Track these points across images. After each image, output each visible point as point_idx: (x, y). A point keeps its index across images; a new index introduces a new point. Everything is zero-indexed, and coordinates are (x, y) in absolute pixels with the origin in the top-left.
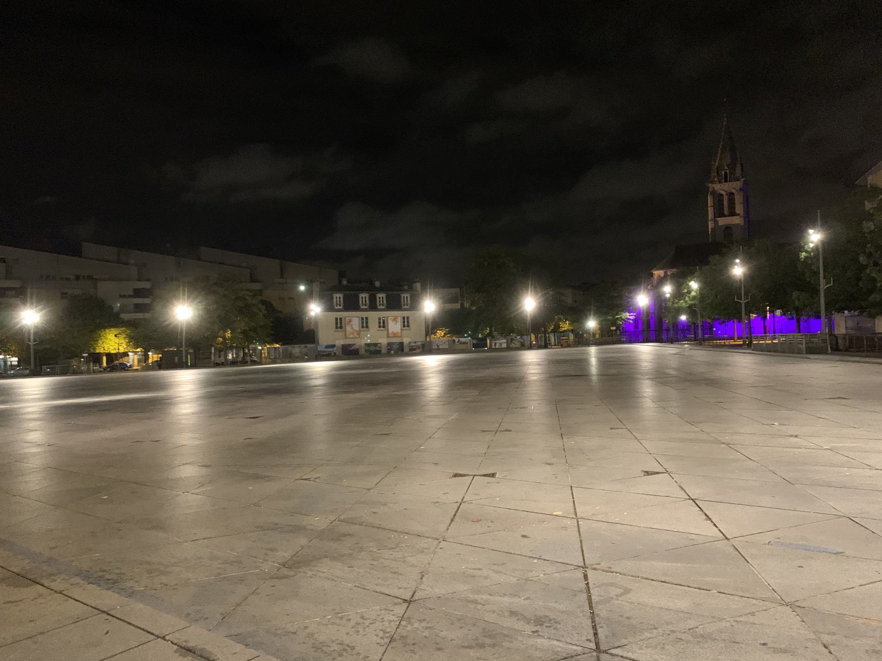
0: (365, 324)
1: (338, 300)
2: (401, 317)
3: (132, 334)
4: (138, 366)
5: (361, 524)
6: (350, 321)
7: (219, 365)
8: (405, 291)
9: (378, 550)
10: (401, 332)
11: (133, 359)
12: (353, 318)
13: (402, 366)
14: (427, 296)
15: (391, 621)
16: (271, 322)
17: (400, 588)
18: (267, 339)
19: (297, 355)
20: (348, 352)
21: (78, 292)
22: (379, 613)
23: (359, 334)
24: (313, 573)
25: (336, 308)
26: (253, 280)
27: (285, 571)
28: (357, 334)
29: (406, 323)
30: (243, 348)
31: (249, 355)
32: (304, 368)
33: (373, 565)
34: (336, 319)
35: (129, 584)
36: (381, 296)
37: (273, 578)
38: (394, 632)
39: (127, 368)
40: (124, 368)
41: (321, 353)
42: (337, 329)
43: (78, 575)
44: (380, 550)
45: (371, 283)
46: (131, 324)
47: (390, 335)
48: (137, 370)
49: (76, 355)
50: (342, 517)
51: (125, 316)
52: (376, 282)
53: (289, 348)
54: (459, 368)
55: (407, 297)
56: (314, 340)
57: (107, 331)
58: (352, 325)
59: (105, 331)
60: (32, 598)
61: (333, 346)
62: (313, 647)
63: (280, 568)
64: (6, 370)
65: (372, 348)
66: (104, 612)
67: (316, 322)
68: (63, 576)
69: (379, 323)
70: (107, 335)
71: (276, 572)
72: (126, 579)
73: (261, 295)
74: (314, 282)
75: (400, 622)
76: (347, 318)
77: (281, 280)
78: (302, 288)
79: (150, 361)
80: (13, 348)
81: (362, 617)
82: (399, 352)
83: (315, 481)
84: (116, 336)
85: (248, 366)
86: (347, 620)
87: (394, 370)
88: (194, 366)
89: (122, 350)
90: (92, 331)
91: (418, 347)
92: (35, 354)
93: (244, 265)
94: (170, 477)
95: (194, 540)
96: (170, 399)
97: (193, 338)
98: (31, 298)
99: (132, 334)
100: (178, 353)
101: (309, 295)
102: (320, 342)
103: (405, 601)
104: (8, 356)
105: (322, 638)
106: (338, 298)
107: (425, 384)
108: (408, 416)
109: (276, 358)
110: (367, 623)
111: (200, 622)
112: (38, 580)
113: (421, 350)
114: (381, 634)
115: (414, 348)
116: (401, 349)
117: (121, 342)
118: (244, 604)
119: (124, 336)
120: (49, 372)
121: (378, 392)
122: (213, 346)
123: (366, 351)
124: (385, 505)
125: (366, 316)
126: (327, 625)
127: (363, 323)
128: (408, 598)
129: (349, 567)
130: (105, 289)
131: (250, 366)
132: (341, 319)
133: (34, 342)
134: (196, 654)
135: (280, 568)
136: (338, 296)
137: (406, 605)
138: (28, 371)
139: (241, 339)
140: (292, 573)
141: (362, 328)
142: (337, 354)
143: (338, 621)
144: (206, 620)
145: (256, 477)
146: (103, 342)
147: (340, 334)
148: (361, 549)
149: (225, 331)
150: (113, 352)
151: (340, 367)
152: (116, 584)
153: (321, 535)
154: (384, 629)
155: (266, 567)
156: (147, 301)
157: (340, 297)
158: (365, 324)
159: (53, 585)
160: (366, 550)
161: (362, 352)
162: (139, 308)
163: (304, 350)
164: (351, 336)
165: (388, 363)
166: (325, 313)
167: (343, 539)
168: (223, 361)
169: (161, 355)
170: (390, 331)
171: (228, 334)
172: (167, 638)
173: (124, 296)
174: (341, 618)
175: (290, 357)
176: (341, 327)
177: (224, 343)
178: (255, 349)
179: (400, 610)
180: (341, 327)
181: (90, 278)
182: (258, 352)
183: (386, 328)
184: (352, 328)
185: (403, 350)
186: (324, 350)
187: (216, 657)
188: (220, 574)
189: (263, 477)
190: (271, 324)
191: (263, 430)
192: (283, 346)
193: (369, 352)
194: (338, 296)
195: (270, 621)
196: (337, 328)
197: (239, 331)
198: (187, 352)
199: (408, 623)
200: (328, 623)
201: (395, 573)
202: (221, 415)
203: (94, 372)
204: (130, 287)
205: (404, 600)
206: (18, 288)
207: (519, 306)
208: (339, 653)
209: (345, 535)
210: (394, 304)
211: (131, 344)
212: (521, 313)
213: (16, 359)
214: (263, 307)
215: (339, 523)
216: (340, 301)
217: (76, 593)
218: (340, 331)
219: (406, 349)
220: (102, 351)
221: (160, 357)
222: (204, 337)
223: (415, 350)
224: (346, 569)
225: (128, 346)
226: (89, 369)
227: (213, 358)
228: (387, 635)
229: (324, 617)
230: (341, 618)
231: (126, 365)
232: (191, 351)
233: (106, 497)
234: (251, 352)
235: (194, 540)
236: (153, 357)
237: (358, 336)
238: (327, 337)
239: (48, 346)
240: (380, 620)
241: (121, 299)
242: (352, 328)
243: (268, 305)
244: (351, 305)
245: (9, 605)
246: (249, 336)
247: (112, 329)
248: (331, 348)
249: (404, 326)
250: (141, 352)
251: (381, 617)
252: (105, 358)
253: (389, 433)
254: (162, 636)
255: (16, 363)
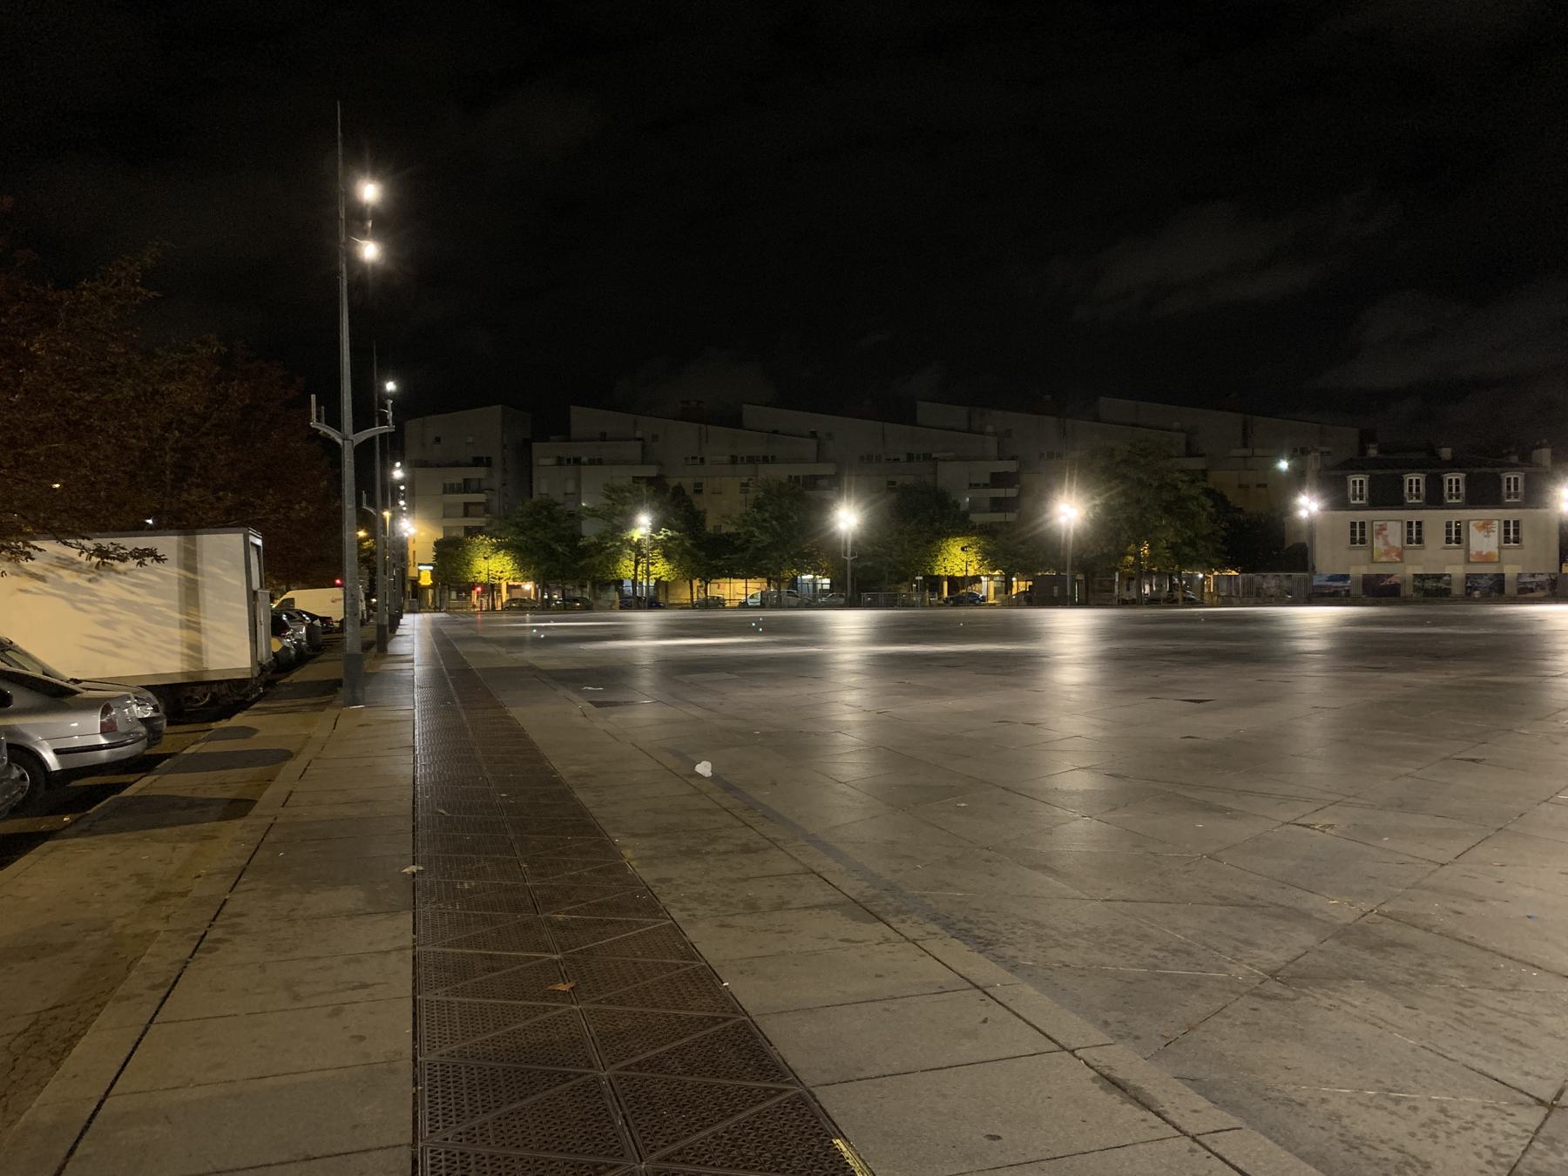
0: (1415, 535)
1: (1358, 487)
2: (1499, 520)
3: (987, 547)
4: (995, 598)
5: (1427, 929)
6: (1383, 528)
7: (1127, 604)
8: (1512, 466)
9: (1470, 987)
10: (1500, 552)
11: (987, 587)
12: (1389, 524)
13: (1504, 624)
14: (1062, 493)
15: (1510, 1134)
16: (1224, 529)
17: (1527, 1074)
18: (1215, 561)
19: (1272, 591)
20: (1376, 590)
21: (909, 480)
22: (1480, 1111)
23: (1400, 555)
24: (1331, 1002)
25: (1352, 502)
26: (1189, 453)
27: (1274, 988)
28: (1396, 556)
29: (1511, 534)
30: (1171, 576)
31: (1180, 589)
32: (1288, 617)
33: (1461, 1014)
34: (1353, 524)
35: (1010, 951)
36: (1456, 479)
37: (1254, 995)
38: (1518, 1157)
39: (977, 602)
40: (975, 601)
41: (1319, 591)
42: (1411, 543)
43: (935, 920)
44: (1474, 987)
45: (1432, 452)
46: (987, 532)
47: (1471, 560)
48: (994, 604)
49: (905, 578)
50: (1386, 909)
51: (977, 518)
52: (1444, 450)
53: (1256, 577)
54: (907, 629)
55: (1516, 479)
56: (1306, 565)
57: (951, 541)
58: (1387, 536)
59: (947, 541)
60: (876, 942)
61: (1345, 577)
62: (1343, 1142)
63: (1266, 980)
64: (815, 597)
65: (1429, 584)
66: (978, 987)
67: (1311, 526)
68: (915, 918)
69: (1449, 532)
70: (950, 547)
71: (1258, 985)
72: (1004, 942)
73: (1205, 481)
74: (1309, 452)
75: (1531, 1142)
76: (1375, 523)
77: (1243, 452)
78: (1284, 465)
79: (1014, 592)
80: (825, 565)
81: (1443, 1111)
82: (1493, 594)
83: (1323, 832)
84: (963, 549)
85: (1178, 607)
86: (1409, 1108)
87: (1482, 631)
88: (1084, 603)
89: (971, 573)
90: (929, 542)
91: (1540, 586)
92: (852, 574)
93: (1176, 425)
94: (1059, 787)
95: (1107, 900)
96: (188, 655)
97: (1084, 556)
98: (850, 484)
99: (987, 547)
100: (1059, 580)
101: (1297, 480)
102: (1318, 569)
103: (1541, 1102)
104: (818, 577)
105: (1360, 1129)
106: (1358, 482)
107: (1560, 664)
108: (1522, 727)
109: (1230, 596)
110: (1454, 1124)
111: (1126, 1041)
112: (882, 916)
113: (1547, 592)
114: (1488, 1155)
115: (1530, 586)
116: (1497, 589)
117: (971, 559)
118: (1202, 1028)
119: (975, 550)
120: (870, 601)
121: (1447, 674)
122: (1117, 569)
123: (1416, 589)
124: (1481, 901)
125: (1362, 521)
126: (1368, 1107)
127: (1410, 533)
128: (1548, 1099)
129: (1406, 1007)
130: (950, 475)
131: (1182, 607)
132: (1362, 525)
133: (852, 556)
134: (1127, 1093)
135: (1266, 980)
136: (1358, 481)
137: (1543, 1111)
138: (843, 600)
139: (1168, 559)
140: (1289, 994)
141: (1505, 542)
142: (1352, 593)
143: (1390, 1105)
144: (1137, 1041)
145: (1208, 808)
146: (944, 559)
147: (1362, 554)
148: (1432, 978)
149: (1139, 544)
150: (958, 575)
151: (1350, 619)
152: (990, 948)
153: (1343, 934)
154: (1495, 1147)
155: (1239, 971)
156: (1012, 493)
157: (1361, 482)
158: (1415, 535)
159: (901, 927)
160: (1442, 981)
161: (1407, 590)
162: (998, 505)
163: (1286, 583)
164: (1384, 559)
165: (1467, 616)
166: (1327, 513)
167: (1389, 949)
168: (1135, 597)
169: (1030, 583)
170: (1473, 552)
171: (1145, 550)
172: (1078, 1053)
173: (977, 485)
174: (1397, 1101)
175: (1258, 595)
176: (1362, 541)
177: (1137, 565)
178: (1191, 579)
179: (1533, 1117)
180: (1362, 541)
181: (927, 457)
182: (1196, 583)
183: (1464, 544)
184: (1386, 543)
185: (1501, 590)
186: (1326, 583)
187: (1161, 1108)
188: (1156, 966)
189: (1223, 810)
190: (1223, 533)
191: (1215, 725)
192: (1244, 575)
193: (1422, 592)
194: (1358, 481)
195: (1253, 1071)
196: (1353, 541)
197: (1164, 543)
198: (1074, 580)
199: (1549, 1147)
200: (1370, 1104)
201: (1513, 1041)
202: (1132, 691)
203: (931, 605)
204: (984, 470)
205: (1538, 1099)
206: (830, 475)
207: (1047, 516)
208: (1396, 1167)
209: (1393, 944)
210: (1484, 494)
211: (985, 562)
212: (834, 534)
213: (827, 581)
214: (1209, 503)
215: (1379, 918)
216: (1361, 490)
217: (934, 945)
218: (1361, 548)
219: (1510, 589)
220: (942, 573)
221: (1030, 586)
222: (1104, 554)
223: (1528, 592)
224: (1402, 1010)
225: (981, 566)
226: (923, 600)
227: (1116, 591)
228: (1503, 1160)
229: (1362, 1090)
230: (1397, 1101)
231: (976, 596)
232: (1080, 577)
233: (963, 805)
234: (1184, 582)
235: (1107, 900)
236: (1019, 586)
237: (1398, 560)
238: (1329, 560)
239: (869, 563)
240: (1484, 1126)
241: (971, 490)
242: (1386, 543)
243: (1218, 498)
244: (1386, 496)
245: (846, 945)
246: (1183, 555)
247: (958, 539)
248: (1341, 580)
249: (1507, 540)
250: (1001, 575)
251: (1485, 1121)
252: (946, 584)
253: (1481, 757)
254: (1070, 1048)
255: (827, 587)
